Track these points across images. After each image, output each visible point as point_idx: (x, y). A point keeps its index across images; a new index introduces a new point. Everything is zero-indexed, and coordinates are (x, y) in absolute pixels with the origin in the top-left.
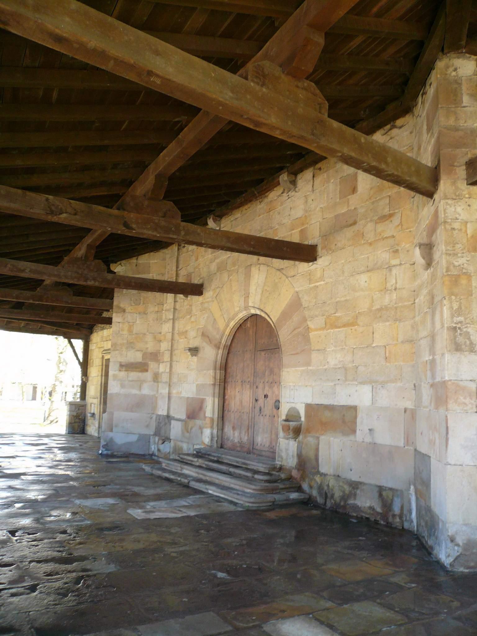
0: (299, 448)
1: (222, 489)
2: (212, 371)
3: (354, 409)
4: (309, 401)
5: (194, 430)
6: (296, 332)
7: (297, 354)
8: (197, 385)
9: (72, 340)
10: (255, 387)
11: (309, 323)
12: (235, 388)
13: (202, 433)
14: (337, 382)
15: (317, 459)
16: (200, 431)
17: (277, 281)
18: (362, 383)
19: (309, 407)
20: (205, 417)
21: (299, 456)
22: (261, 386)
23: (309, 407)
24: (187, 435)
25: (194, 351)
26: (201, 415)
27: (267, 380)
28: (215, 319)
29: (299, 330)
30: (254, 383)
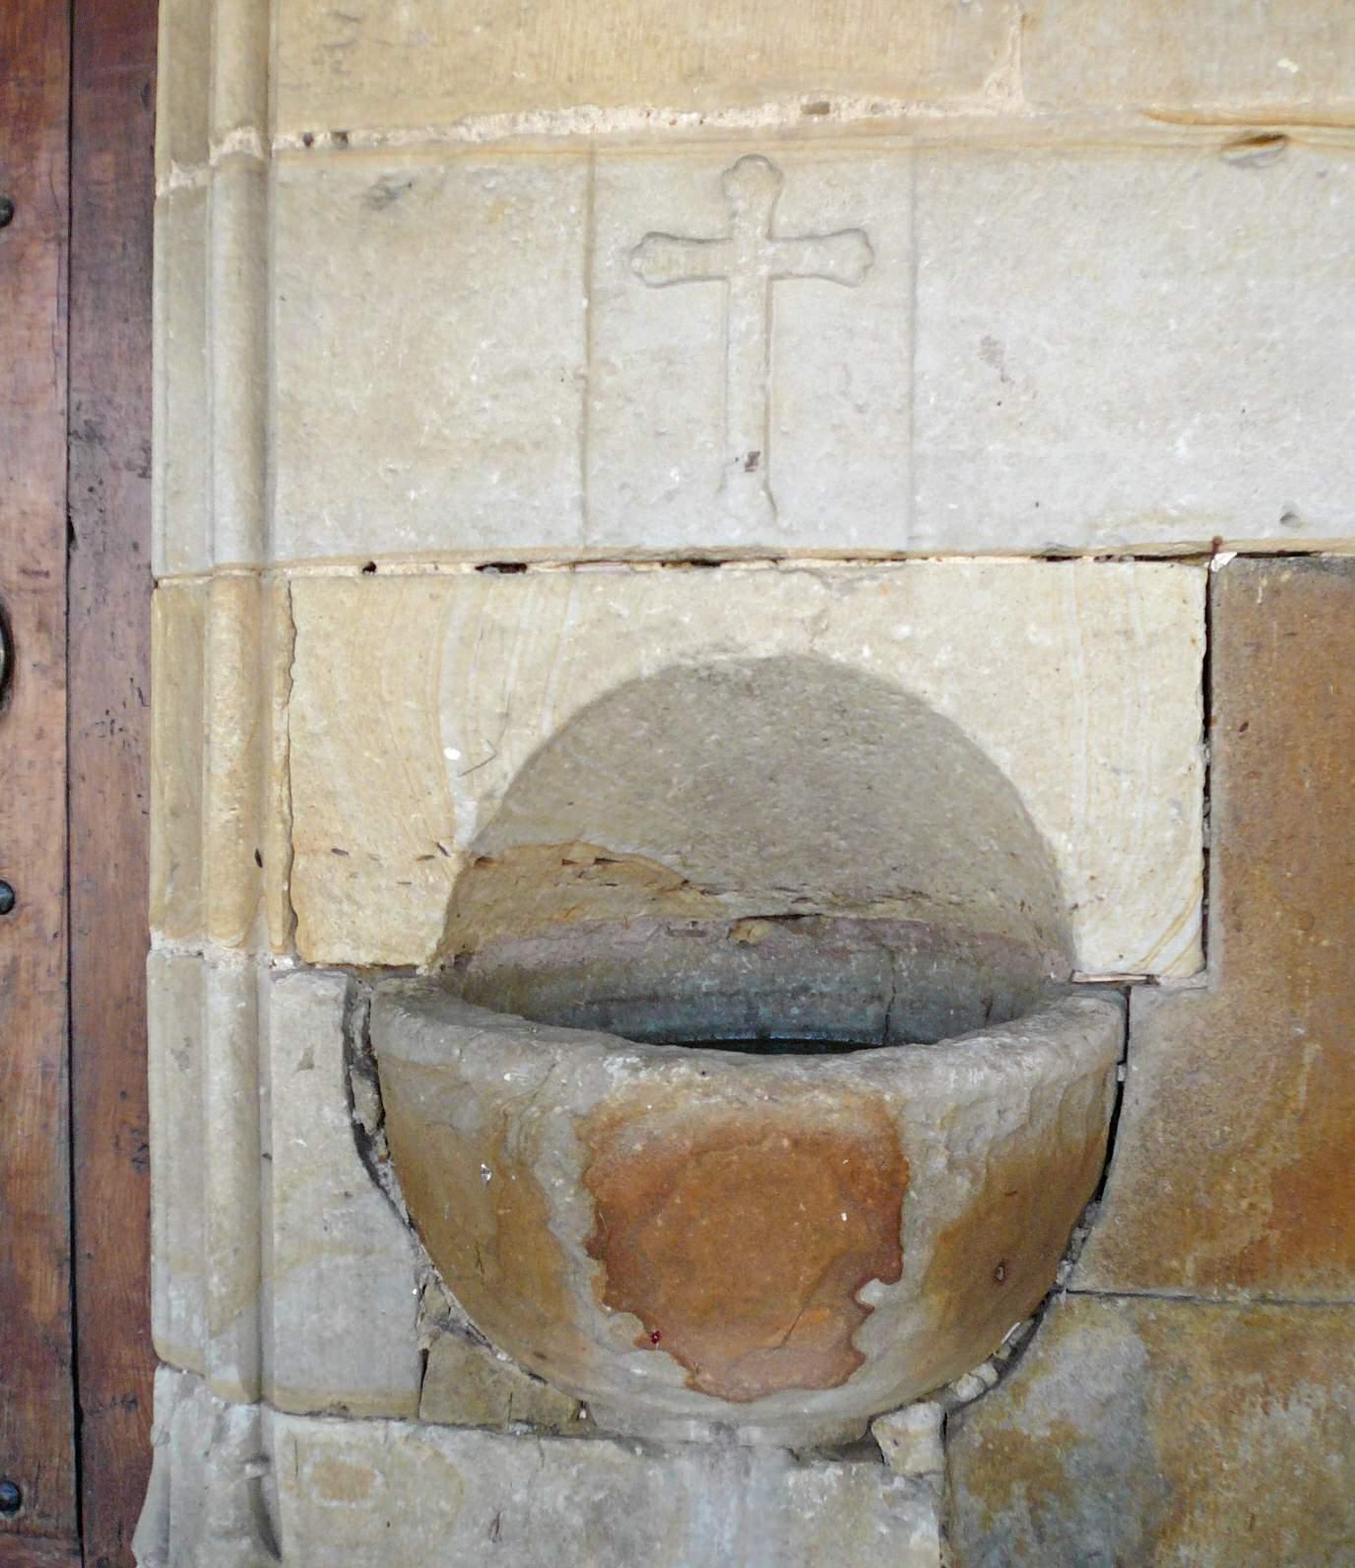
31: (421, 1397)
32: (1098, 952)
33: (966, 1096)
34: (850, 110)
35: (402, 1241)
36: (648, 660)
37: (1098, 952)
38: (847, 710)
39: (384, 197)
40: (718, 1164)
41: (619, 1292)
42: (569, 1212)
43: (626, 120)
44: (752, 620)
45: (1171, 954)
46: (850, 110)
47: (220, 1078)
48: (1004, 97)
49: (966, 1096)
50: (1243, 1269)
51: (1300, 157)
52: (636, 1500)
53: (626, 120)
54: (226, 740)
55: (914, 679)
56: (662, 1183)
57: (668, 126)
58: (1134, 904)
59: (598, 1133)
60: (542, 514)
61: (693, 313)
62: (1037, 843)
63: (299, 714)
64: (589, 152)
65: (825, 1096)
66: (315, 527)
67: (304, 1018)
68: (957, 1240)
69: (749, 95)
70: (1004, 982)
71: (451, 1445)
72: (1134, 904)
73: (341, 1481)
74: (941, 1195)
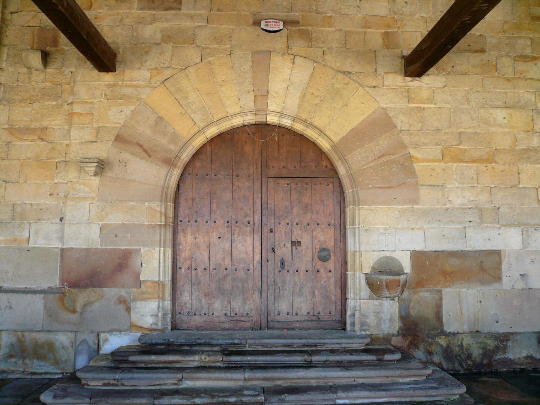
20: (138, 283)
31: (370, 298)
32: (406, 271)
33: (402, 278)
34: (392, 226)
35: (368, 289)
36: (382, 256)
37: (406, 271)
38: (391, 258)
39: (366, 230)
40: (392, 281)
41: (387, 288)
42: (384, 284)
43: (380, 226)
44: (388, 254)
45: (409, 272)
46: (392, 226)
47: (358, 280)
48: (400, 226)
49: (402, 278)
50: (414, 288)
51: (415, 230)
52: (382, 303)
53: (380, 226)
54: (358, 261)
55: (396, 257)
56: (390, 282)
57: (147, 59)
58: (407, 269)
59: (386, 280)
60: (375, 248)
61: (384, 237)
62: (402, 266)
63: (362, 259)
64: (378, 228)
65: (397, 278)
66: (363, 249)
67: (363, 277)
68: (402, 285)
69: (386, 225)
70: (400, 272)
71: (371, 301)
72: (407, 269)
73: (365, 304)
74: (401, 283)
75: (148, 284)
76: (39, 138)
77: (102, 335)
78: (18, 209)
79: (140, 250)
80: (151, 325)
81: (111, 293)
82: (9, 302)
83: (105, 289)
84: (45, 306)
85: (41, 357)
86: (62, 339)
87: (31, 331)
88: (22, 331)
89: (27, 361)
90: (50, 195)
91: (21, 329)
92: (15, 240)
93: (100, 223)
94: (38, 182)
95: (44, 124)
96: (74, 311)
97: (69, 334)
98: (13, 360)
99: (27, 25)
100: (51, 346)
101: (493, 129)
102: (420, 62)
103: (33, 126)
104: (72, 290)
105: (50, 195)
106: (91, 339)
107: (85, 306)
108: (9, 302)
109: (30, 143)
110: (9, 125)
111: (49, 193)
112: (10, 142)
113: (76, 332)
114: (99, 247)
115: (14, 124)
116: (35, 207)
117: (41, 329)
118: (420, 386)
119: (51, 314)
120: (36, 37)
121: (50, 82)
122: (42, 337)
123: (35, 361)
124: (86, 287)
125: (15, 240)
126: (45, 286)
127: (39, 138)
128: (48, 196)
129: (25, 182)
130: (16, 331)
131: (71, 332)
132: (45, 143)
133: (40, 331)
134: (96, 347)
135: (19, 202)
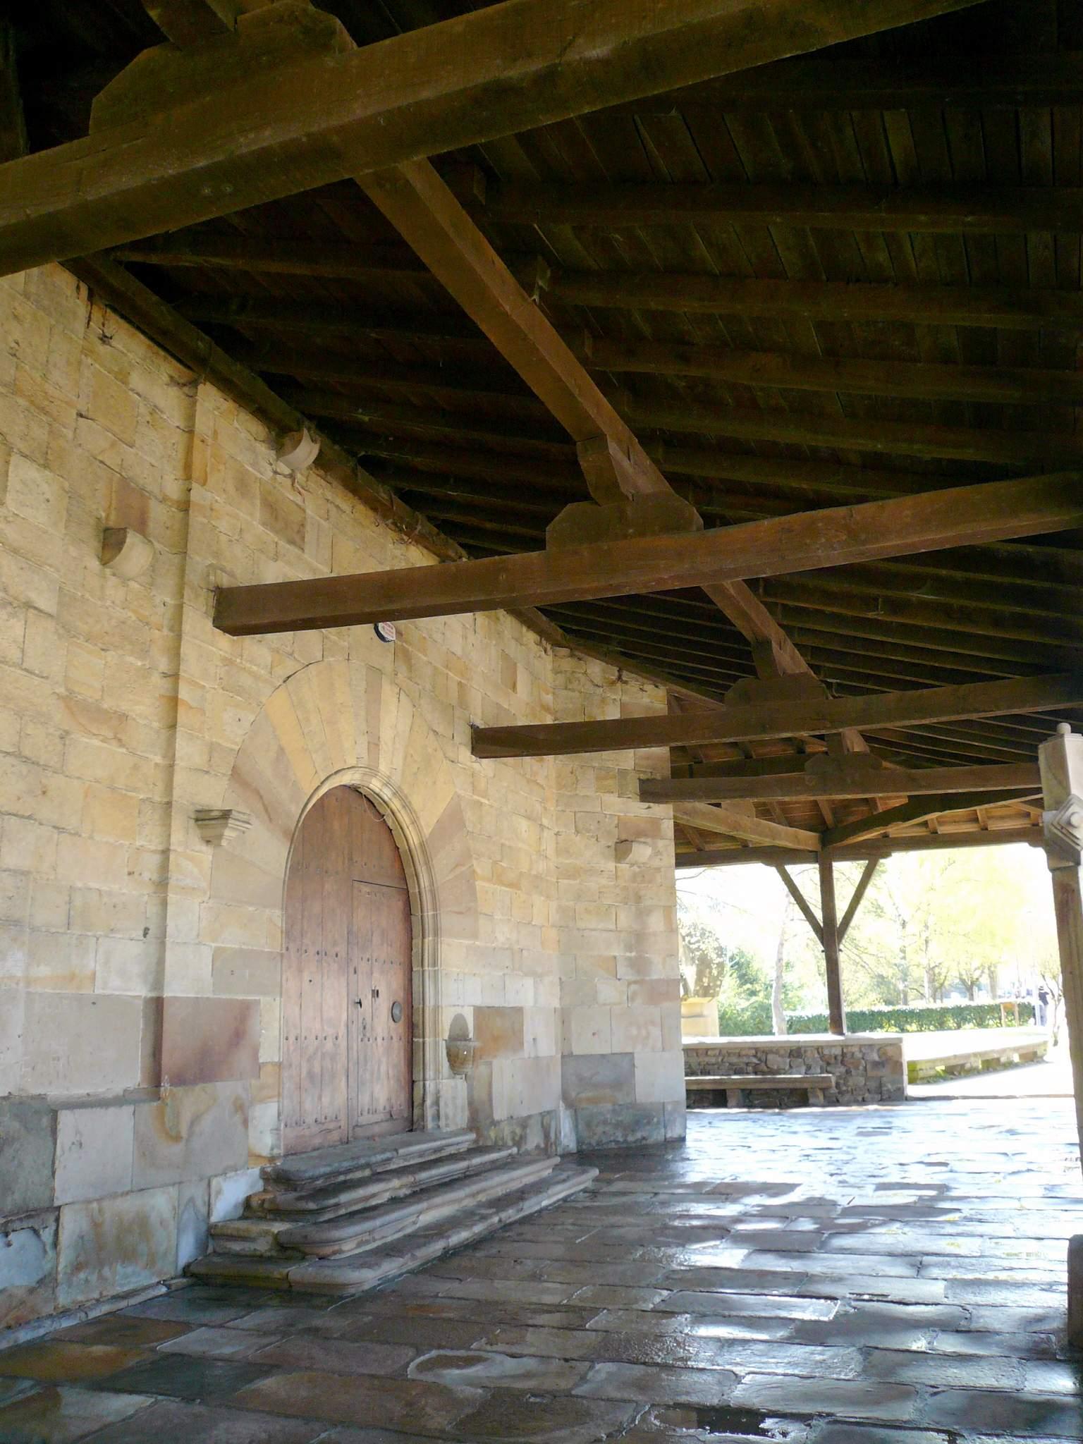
0: (470, 1089)
1: (929, 1082)
2: (278, 912)
3: (519, 1010)
4: (478, 1003)
5: (206, 1123)
6: (458, 871)
7: (461, 913)
8: (217, 954)
9: (380, 625)
10: (352, 970)
11: (475, 862)
12: (300, 971)
13: (245, 1122)
14: (506, 971)
15: (490, 1100)
16: (238, 1118)
17: (430, 750)
18: (526, 975)
19: (479, 1011)
20: (258, 1067)
21: (471, 1103)
22: (363, 967)
23: (479, 1011)
24: (175, 1151)
25: (210, 821)
26: (242, 1058)
27: (375, 955)
28: (281, 750)
29: (463, 869)
30: (349, 960)
75: (269, 1068)
76: (115, 738)
77: (214, 1182)
78: (78, 902)
79: (258, 1002)
80: (272, 1149)
81: (226, 1089)
82: (78, 1132)
83: (219, 1084)
84: (136, 1132)
85: (128, 1255)
86: (160, 1203)
87: (114, 1196)
88: (99, 1200)
89: (106, 1272)
90: (130, 874)
91: (97, 1196)
92: (72, 977)
93: (213, 945)
94: (112, 840)
95: (124, 707)
96: (177, 1138)
97: (171, 1189)
98: (82, 1275)
99: (100, 458)
100: (142, 1225)
101: (520, 845)
102: (493, 742)
103: (105, 706)
104: (175, 1089)
105: (130, 874)
106: (198, 1192)
107: (192, 1124)
108: (78, 1132)
109: (100, 744)
110: (67, 690)
111: (126, 871)
112: (67, 732)
113: (180, 1183)
114: (211, 995)
115: (76, 689)
116: (105, 899)
117: (128, 1188)
118: (343, 1211)
119: (145, 1152)
120: (114, 495)
121: (134, 611)
122: (128, 1206)
123: (119, 1267)
124: (194, 1082)
125: (72, 977)
126: (117, 1089)
127: (115, 738)
128: (126, 877)
129: (91, 837)
130: (89, 1202)
131: (174, 1184)
132: (124, 750)
133: (127, 1193)
134: (204, 1210)
135: (79, 885)
